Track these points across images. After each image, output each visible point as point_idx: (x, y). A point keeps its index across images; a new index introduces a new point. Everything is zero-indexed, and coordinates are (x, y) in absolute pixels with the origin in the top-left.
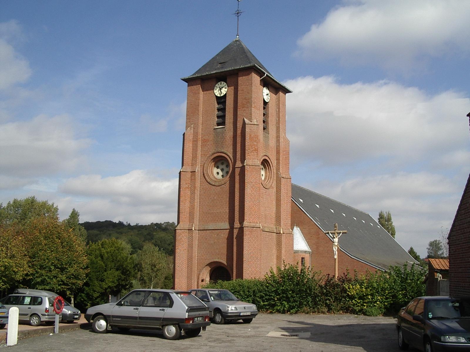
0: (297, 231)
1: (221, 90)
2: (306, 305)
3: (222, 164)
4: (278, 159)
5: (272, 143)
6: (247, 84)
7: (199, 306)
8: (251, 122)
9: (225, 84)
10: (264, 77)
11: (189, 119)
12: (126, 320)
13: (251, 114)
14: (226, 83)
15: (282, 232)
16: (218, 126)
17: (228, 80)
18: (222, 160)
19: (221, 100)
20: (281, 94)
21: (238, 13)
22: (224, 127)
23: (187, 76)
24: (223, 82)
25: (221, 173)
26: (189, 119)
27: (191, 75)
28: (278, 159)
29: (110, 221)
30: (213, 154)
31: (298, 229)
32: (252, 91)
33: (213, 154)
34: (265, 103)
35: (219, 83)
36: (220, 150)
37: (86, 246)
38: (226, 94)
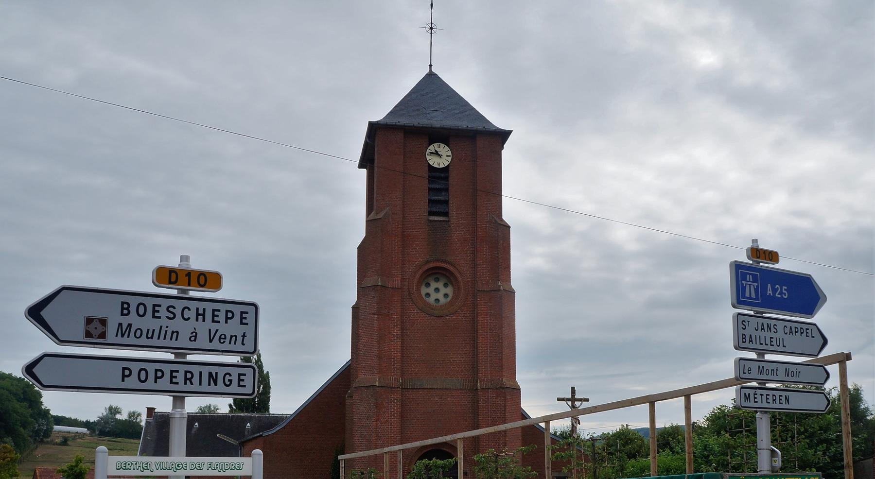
3: (437, 280)
9: (447, 148)
19: (438, 175)
24: (442, 145)
25: (440, 285)
30: (427, 262)
33: (427, 262)
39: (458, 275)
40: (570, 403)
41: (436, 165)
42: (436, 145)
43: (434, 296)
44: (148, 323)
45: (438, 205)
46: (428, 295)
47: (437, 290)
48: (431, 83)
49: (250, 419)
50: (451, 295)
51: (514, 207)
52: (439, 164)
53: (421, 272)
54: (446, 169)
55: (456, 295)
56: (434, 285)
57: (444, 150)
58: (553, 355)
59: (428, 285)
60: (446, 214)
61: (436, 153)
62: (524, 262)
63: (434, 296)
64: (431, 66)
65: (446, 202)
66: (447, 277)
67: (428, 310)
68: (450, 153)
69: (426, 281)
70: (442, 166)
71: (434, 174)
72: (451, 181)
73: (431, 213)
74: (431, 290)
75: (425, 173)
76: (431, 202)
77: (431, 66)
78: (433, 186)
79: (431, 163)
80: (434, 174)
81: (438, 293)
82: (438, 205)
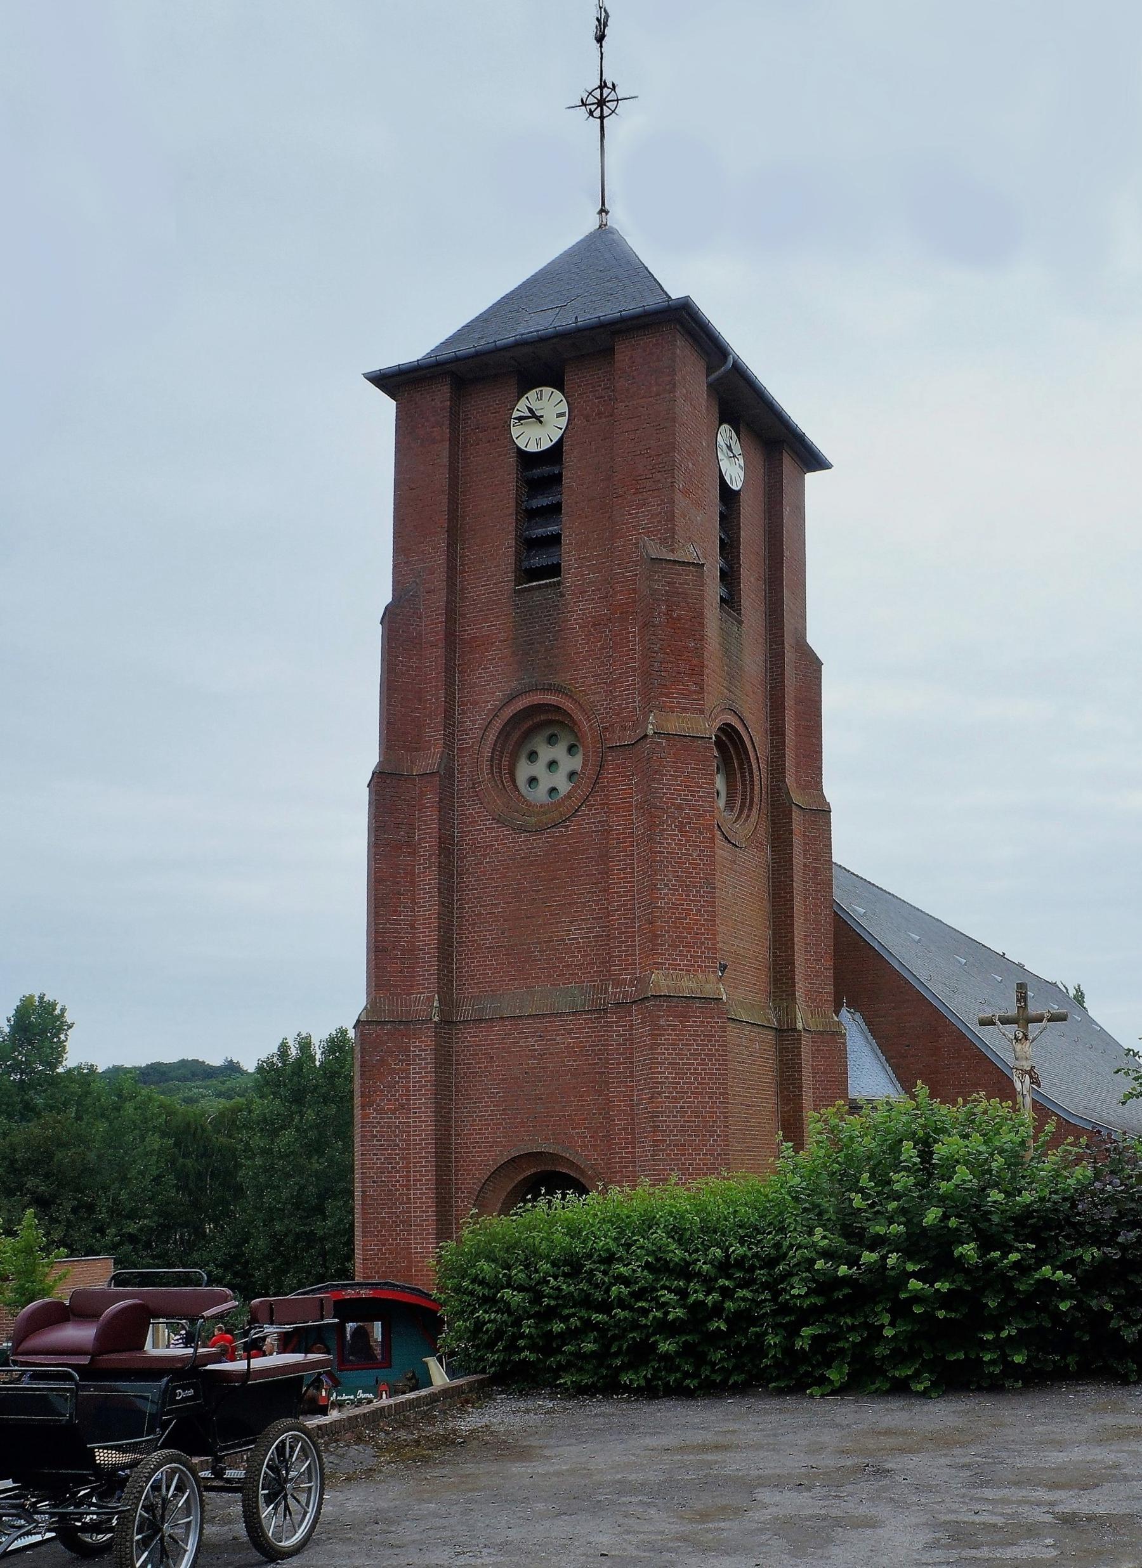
0: (851, 1024)
1: (542, 420)
2: (250, 1112)
3: (552, 740)
4: (777, 732)
5: (753, 662)
8: (672, 551)
9: (558, 395)
12: (789, 716)
13: (671, 518)
14: (562, 390)
15: (800, 1026)
17: (569, 378)
18: (550, 723)
19: (541, 471)
24: (547, 390)
25: (558, 752)
28: (777, 732)
29: (196, 1062)
30: (511, 699)
31: (857, 1015)
32: (674, 420)
33: (511, 699)
34: (728, 495)
38: (561, 439)
40: (1033, 1010)
41: (532, 448)
42: (532, 394)
44: (428, 827)
45: (538, 559)
47: (552, 765)
48: (602, 252)
52: (539, 442)
53: (498, 725)
54: (555, 453)
56: (546, 753)
59: (533, 756)
61: (535, 416)
64: (603, 211)
68: (564, 407)
69: (528, 748)
70: (546, 445)
71: (537, 472)
72: (569, 479)
74: (539, 769)
77: (603, 211)
79: (521, 443)
82: (538, 559)
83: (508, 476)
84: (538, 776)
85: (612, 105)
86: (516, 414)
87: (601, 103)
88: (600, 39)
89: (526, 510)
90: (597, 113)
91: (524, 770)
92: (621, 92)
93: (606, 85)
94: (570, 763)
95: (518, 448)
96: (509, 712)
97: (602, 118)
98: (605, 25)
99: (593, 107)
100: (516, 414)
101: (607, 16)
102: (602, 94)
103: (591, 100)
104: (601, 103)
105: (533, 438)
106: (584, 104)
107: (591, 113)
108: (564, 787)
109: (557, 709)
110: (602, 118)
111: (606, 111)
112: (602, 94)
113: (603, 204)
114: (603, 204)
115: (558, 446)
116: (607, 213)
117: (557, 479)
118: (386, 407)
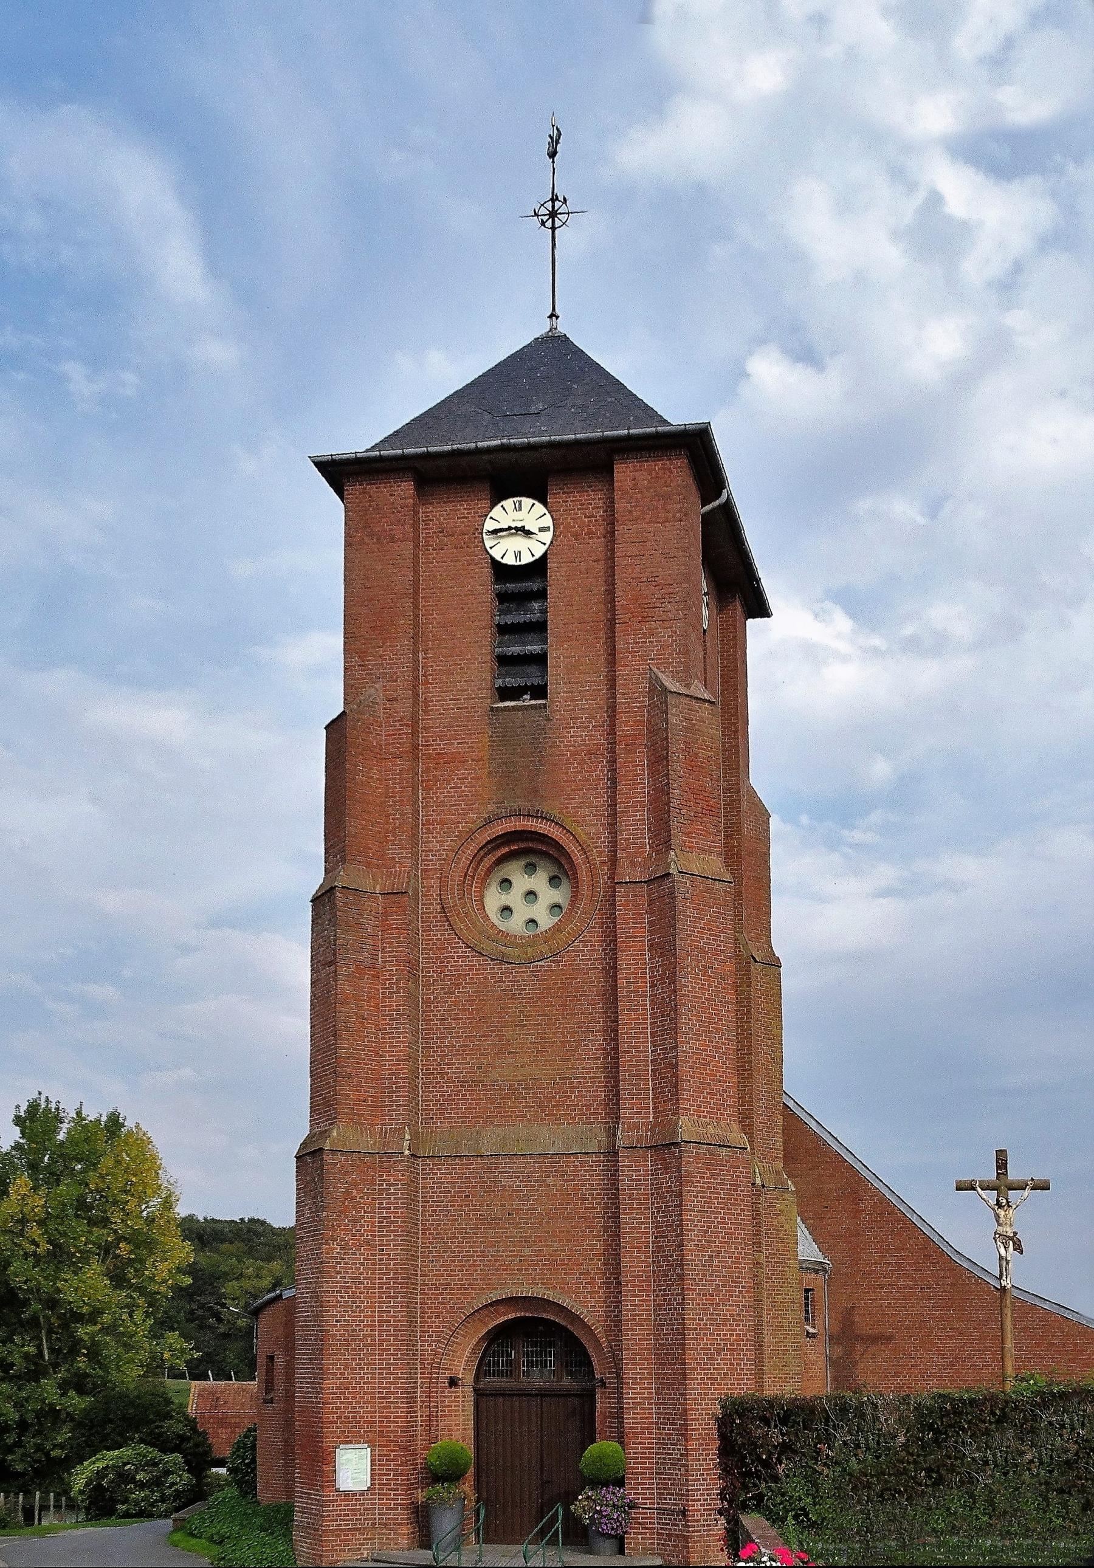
1: (518, 532)
3: (531, 868)
6: (662, 515)
7: (321, 1340)
9: (540, 508)
10: (717, 503)
11: (363, 654)
14: (545, 503)
16: (503, 699)
19: (520, 585)
20: (737, 608)
21: (552, 215)
22: (539, 706)
23: (359, 439)
24: (527, 502)
26: (363, 654)
27: (369, 447)
30: (488, 822)
33: (488, 822)
35: (508, 503)
36: (521, 804)
37: (155, 1337)
38: (545, 555)
39: (555, 832)
41: (510, 560)
43: (522, 912)
45: (521, 672)
46: (506, 910)
49: (39, 1347)
50: (565, 904)
51: (781, 943)
52: (518, 555)
53: (471, 849)
54: (539, 567)
55: (575, 896)
56: (522, 882)
57: (529, 513)
58: (211, 650)
60: (540, 692)
62: (792, 984)
63: (522, 912)
64: (553, 316)
65: (541, 660)
66: (560, 866)
67: (501, 951)
70: (526, 559)
73: (505, 693)
74: (514, 898)
75: (484, 588)
76: (504, 661)
77: (553, 316)
78: (509, 619)
79: (496, 553)
80: (511, 586)
81: (525, 903)
82: (521, 672)
83: (482, 590)
84: (515, 912)
85: (564, 217)
86: (489, 525)
87: (553, 214)
88: (552, 155)
89: (498, 626)
90: (549, 224)
91: (494, 899)
92: (571, 206)
93: (557, 199)
94: (549, 895)
95: (492, 558)
96: (487, 836)
97: (553, 228)
98: (557, 142)
99: (545, 218)
100: (489, 525)
101: (559, 134)
102: (553, 207)
103: (543, 211)
104: (553, 214)
105: (513, 551)
106: (536, 215)
107: (543, 223)
108: (546, 921)
109: (543, 838)
110: (553, 228)
111: (558, 223)
112: (553, 207)
113: (554, 309)
114: (554, 309)
115: (543, 560)
116: (557, 317)
117: (542, 595)
118: (329, 510)
